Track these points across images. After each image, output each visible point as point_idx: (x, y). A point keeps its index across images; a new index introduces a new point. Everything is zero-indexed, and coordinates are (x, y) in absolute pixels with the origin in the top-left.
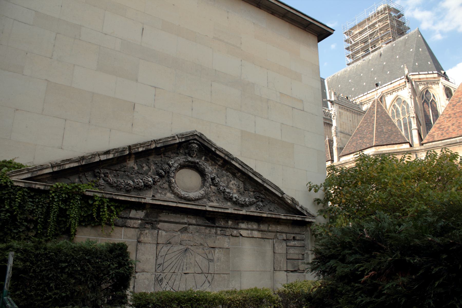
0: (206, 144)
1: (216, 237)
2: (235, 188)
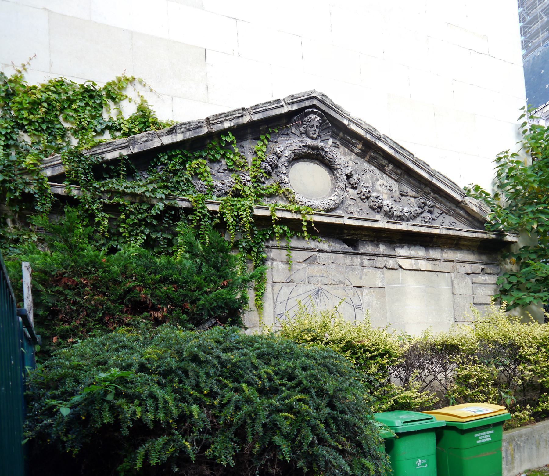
0: (333, 114)
1: (362, 270)
2: (384, 190)
